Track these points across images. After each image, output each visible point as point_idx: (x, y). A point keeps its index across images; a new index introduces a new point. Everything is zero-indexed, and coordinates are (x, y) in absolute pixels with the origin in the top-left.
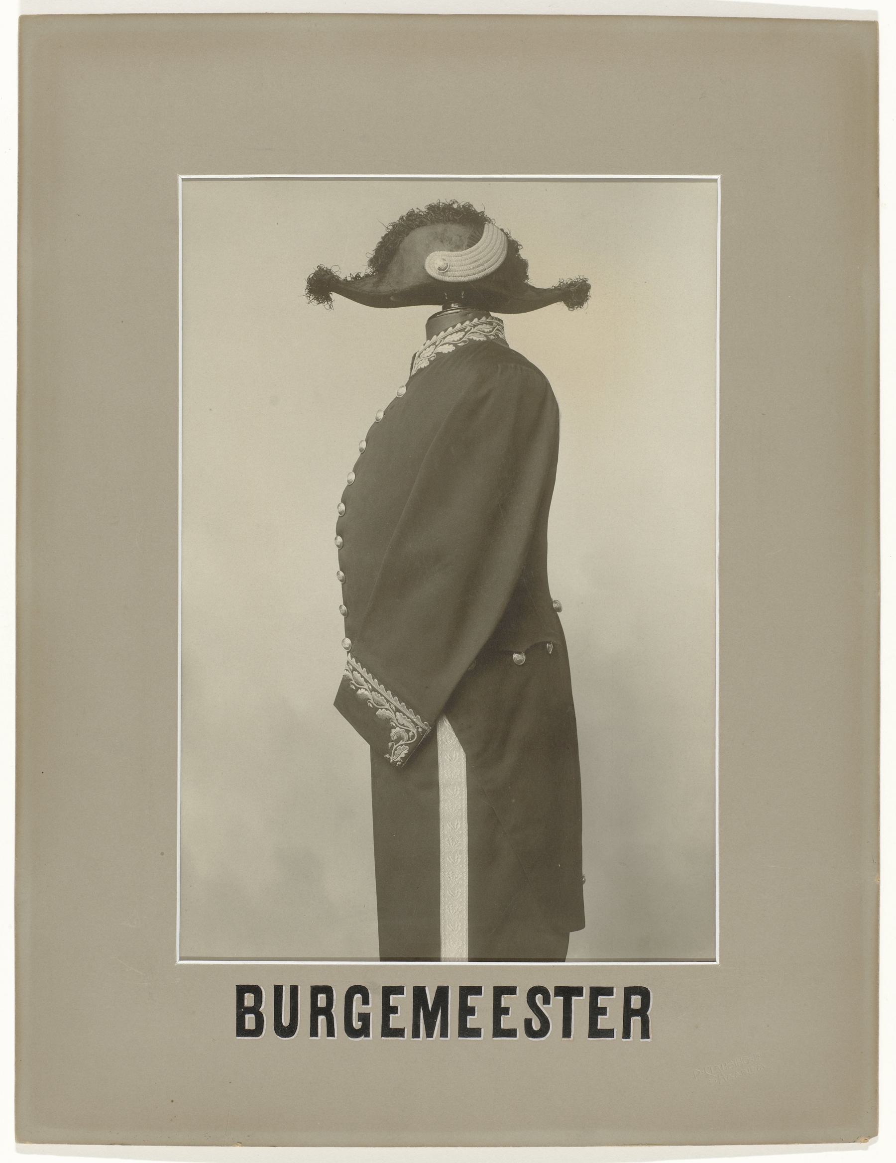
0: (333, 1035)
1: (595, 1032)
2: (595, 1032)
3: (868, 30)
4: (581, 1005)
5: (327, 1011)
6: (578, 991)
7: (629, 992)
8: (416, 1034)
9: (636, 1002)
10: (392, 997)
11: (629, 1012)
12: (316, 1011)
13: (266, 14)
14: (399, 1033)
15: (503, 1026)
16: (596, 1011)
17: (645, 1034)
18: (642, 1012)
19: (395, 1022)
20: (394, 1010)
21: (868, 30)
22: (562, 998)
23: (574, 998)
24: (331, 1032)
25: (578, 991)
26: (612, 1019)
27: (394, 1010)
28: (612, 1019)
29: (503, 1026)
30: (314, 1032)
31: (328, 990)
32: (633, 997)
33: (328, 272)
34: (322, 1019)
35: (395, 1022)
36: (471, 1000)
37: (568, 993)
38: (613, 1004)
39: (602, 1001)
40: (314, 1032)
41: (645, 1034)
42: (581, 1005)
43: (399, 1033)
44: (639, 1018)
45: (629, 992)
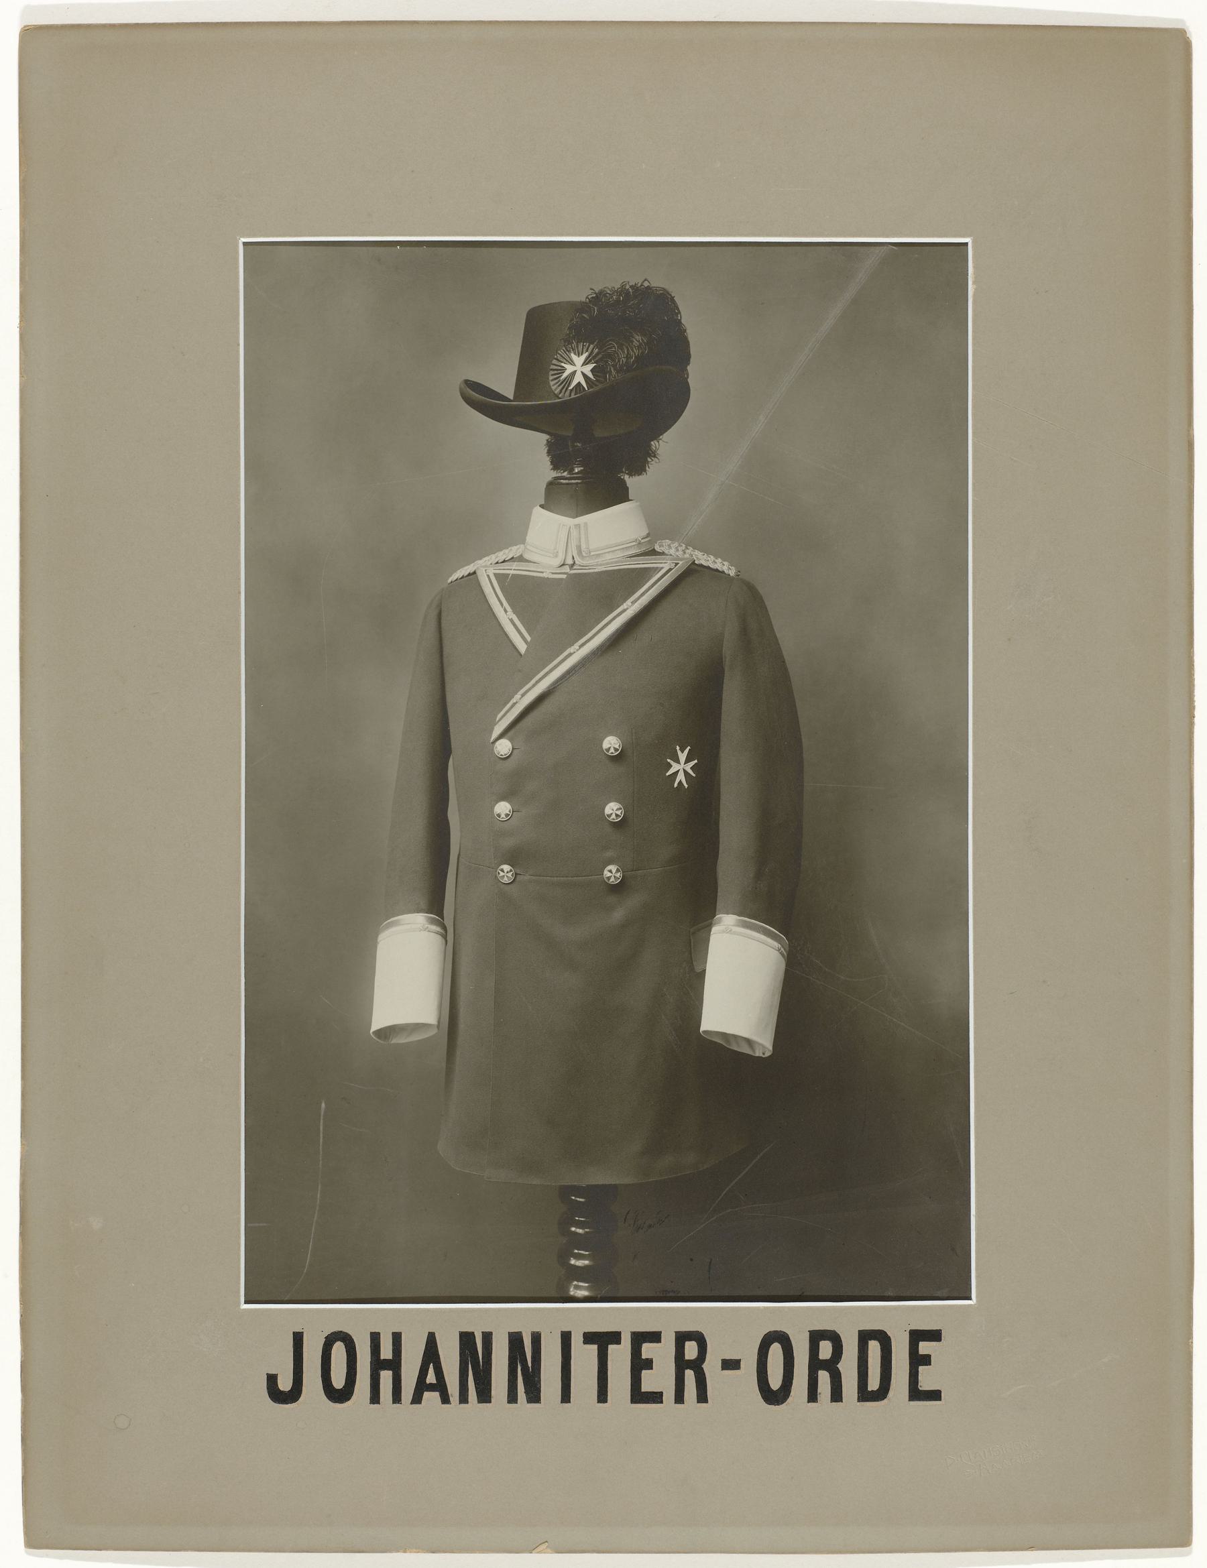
0: (706, 1401)
1: (639, 1396)
2: (639, 1396)
3: (36, 1538)
4: (620, 1356)
5: (832, 1366)
6: (615, 1337)
7: (682, 1338)
8: (679, 1398)
9: (691, 1350)
10: (921, 1344)
11: (681, 1364)
12: (815, 1364)
13: (137, 24)
14: (656, 1398)
15: (646, 1387)
16: (639, 1365)
17: (702, 1397)
18: (697, 1365)
19: (649, 1382)
20: (649, 1364)
21: (36, 1538)
22: (596, 1347)
23: (611, 1347)
24: (837, 1395)
25: (615, 1337)
26: (659, 1378)
27: (649, 1364)
28: (659, 1378)
29: (646, 1387)
30: (813, 1396)
31: (835, 1339)
32: (687, 1343)
33: (1187, 46)
34: (386, 1376)
35: (649, 1382)
36: (924, 1347)
37: (603, 1340)
38: (662, 1354)
39: (647, 1350)
40: (813, 1396)
41: (702, 1397)
42: (620, 1356)
43: (656, 1398)
44: (390, 1373)
45: (682, 1338)
